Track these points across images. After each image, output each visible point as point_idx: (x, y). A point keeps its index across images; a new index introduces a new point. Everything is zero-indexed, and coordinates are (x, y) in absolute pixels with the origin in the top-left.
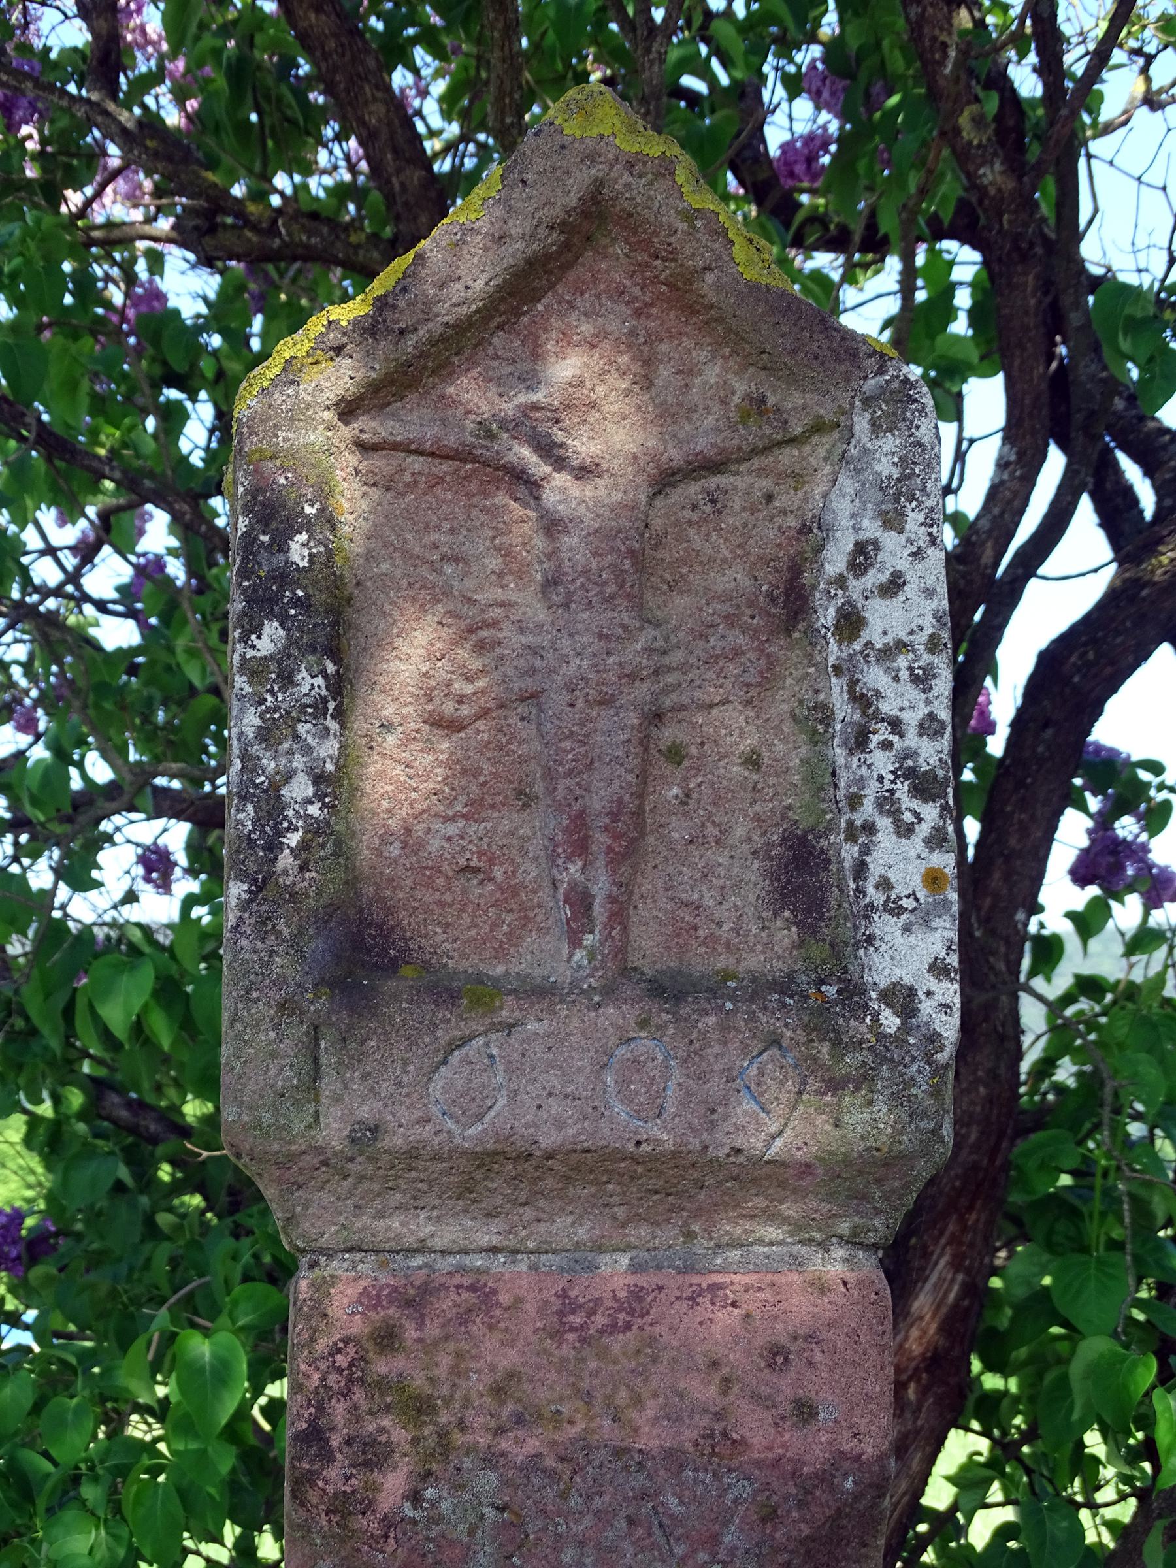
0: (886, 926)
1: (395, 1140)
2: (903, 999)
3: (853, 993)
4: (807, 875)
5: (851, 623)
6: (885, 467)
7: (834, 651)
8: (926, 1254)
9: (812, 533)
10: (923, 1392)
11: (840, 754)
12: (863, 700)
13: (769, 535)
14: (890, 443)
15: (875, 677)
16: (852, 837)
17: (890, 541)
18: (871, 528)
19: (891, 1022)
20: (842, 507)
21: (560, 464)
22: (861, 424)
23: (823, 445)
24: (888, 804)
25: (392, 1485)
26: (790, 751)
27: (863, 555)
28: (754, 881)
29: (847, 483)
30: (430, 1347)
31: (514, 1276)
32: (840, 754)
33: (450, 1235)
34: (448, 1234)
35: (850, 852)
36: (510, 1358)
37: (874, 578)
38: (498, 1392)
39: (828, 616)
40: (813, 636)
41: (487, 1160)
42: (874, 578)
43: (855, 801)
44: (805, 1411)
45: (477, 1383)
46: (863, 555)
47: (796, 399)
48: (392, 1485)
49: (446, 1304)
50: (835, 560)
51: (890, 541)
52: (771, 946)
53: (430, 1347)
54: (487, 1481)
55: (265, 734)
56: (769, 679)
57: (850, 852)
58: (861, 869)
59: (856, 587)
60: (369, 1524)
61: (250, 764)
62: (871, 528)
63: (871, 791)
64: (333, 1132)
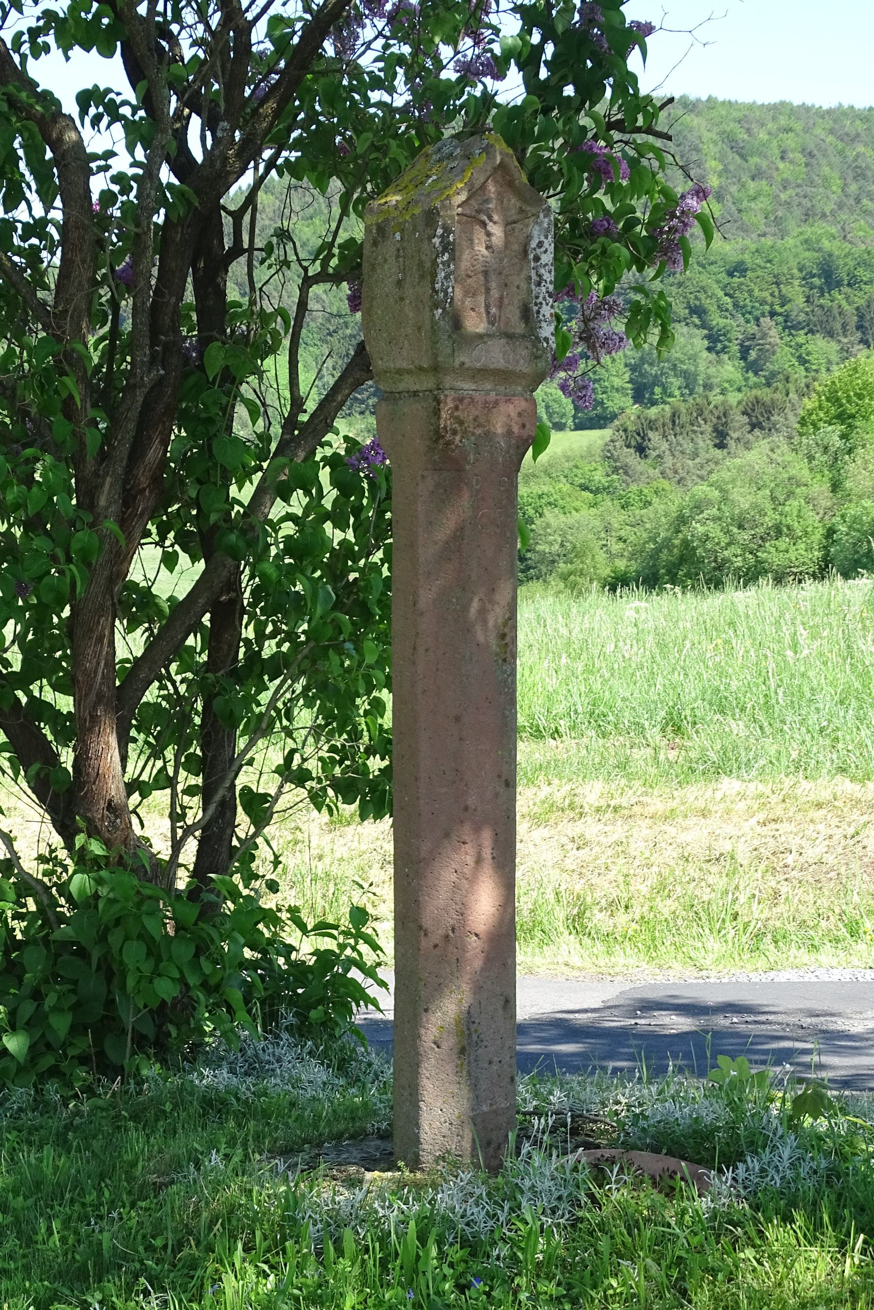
0: (544, 324)
1: (466, 366)
2: (546, 339)
3: (538, 339)
4: (527, 314)
5: (537, 259)
6: (546, 225)
7: (533, 264)
8: (150, 438)
9: (529, 238)
10: (151, 492)
11: (533, 287)
12: (540, 276)
13: (522, 238)
14: (546, 220)
15: (542, 271)
16: (536, 304)
17: (546, 241)
18: (542, 238)
19: (545, 345)
20: (535, 233)
21: (491, 220)
22: (541, 215)
23: (533, 218)
24: (544, 298)
25: (458, 438)
26: (524, 285)
27: (540, 244)
28: (518, 313)
29: (537, 227)
30: (463, 410)
31: (478, 397)
32: (533, 287)
33: (467, 386)
34: (466, 386)
35: (535, 308)
36: (476, 413)
37: (543, 249)
38: (475, 420)
39: (531, 256)
40: (529, 262)
41: (480, 370)
42: (543, 249)
43: (537, 297)
44: (524, 426)
45: (471, 418)
46: (540, 244)
47: (528, 208)
48: (458, 438)
49: (466, 401)
50: (533, 244)
51: (546, 241)
52: (520, 328)
53: (463, 410)
54: (473, 438)
55: (445, 278)
56: (521, 269)
57: (535, 308)
58: (538, 312)
59: (538, 251)
60: (453, 447)
61: (443, 285)
62: (542, 238)
63: (541, 296)
64: (457, 363)
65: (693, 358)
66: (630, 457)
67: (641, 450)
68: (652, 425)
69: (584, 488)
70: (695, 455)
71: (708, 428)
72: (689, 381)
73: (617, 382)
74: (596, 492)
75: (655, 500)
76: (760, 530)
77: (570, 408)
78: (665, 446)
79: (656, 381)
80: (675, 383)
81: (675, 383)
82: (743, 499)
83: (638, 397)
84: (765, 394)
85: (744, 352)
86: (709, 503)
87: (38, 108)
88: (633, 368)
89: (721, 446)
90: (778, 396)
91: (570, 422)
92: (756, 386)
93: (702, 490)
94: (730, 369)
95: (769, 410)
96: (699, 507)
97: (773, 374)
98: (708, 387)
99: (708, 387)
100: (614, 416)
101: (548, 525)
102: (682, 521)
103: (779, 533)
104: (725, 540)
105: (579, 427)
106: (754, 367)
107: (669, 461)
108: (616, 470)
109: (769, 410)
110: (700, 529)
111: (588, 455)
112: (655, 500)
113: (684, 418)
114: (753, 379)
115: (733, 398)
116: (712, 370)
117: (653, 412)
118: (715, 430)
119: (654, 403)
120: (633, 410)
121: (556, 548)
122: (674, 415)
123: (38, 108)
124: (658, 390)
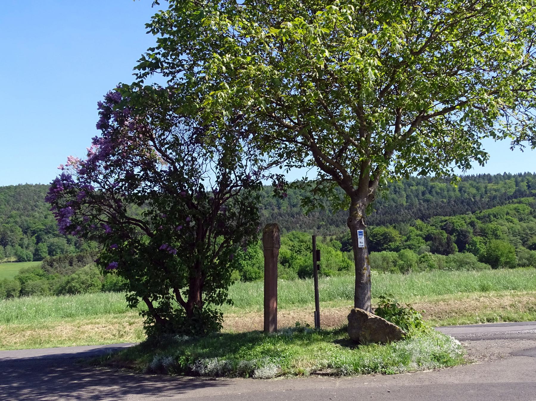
65: (64, 245)
66: (49, 268)
67: (51, 266)
68: (54, 260)
69: (38, 275)
70: (65, 267)
71: (68, 261)
72: (62, 251)
73: (44, 250)
74: (40, 276)
75: (55, 278)
76: (87, 285)
77: (32, 256)
78: (57, 265)
79: (54, 250)
80: (59, 251)
81: (59, 251)
82: (83, 277)
83: (49, 254)
84: (82, 254)
85: (75, 244)
86: (76, 279)
87: (126, 243)
88: (49, 247)
89: (71, 265)
90: (85, 254)
91: (32, 259)
92: (78, 252)
93: (74, 275)
94: (72, 248)
95: (82, 257)
96: (73, 279)
97: (82, 249)
98: (67, 252)
99: (67, 252)
100: (43, 258)
101: (29, 284)
102: (68, 282)
103: (91, 286)
104: (79, 287)
105: (34, 261)
106: (77, 248)
107: (59, 269)
108: (45, 271)
109: (82, 257)
110: (74, 284)
111: (38, 267)
112: (55, 278)
113: (62, 259)
114: (77, 250)
115: (74, 255)
116: (68, 248)
117: (54, 257)
118: (70, 262)
119: (53, 256)
120: (48, 257)
121: (30, 289)
122: (60, 258)
123: (126, 243)
124: (54, 252)
